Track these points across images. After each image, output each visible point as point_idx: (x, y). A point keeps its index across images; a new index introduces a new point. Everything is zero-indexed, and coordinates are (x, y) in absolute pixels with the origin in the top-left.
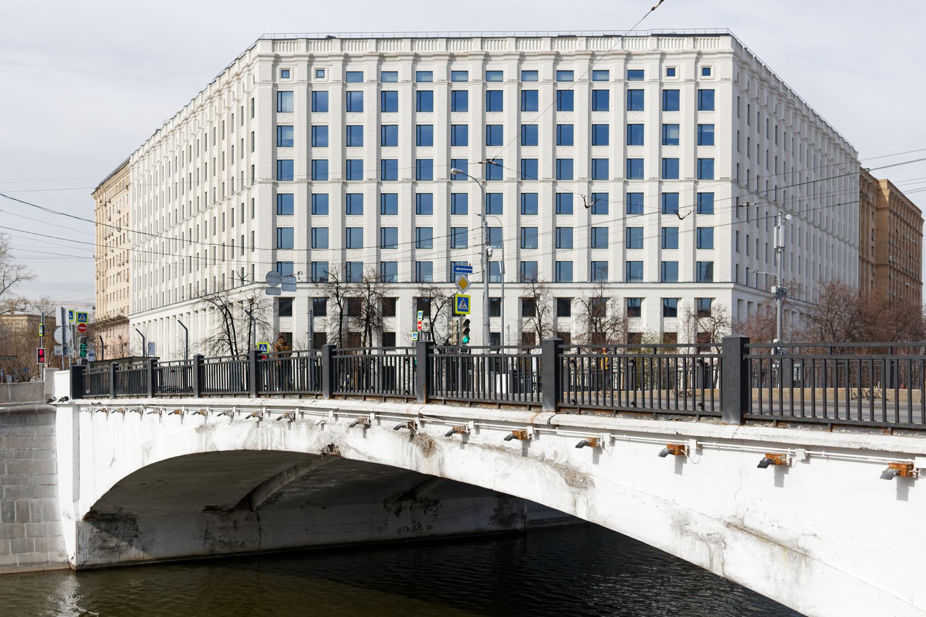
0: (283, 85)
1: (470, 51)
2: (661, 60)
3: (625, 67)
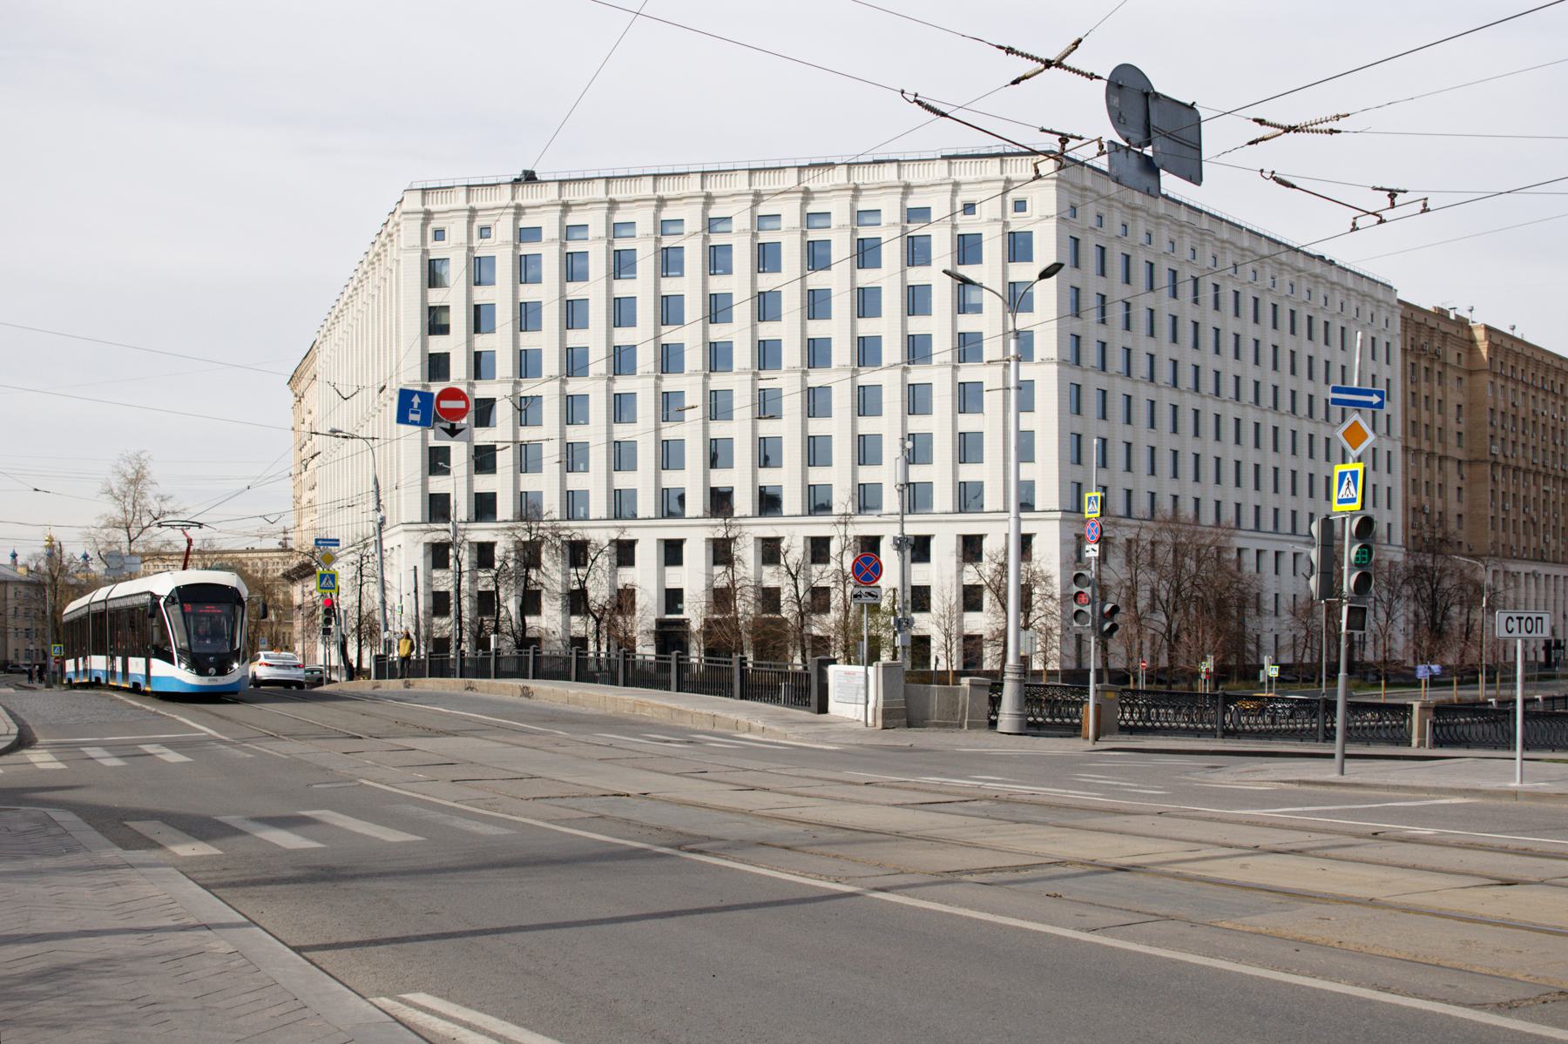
0: (437, 250)
1: (686, 192)
2: (954, 193)
3: (902, 205)
